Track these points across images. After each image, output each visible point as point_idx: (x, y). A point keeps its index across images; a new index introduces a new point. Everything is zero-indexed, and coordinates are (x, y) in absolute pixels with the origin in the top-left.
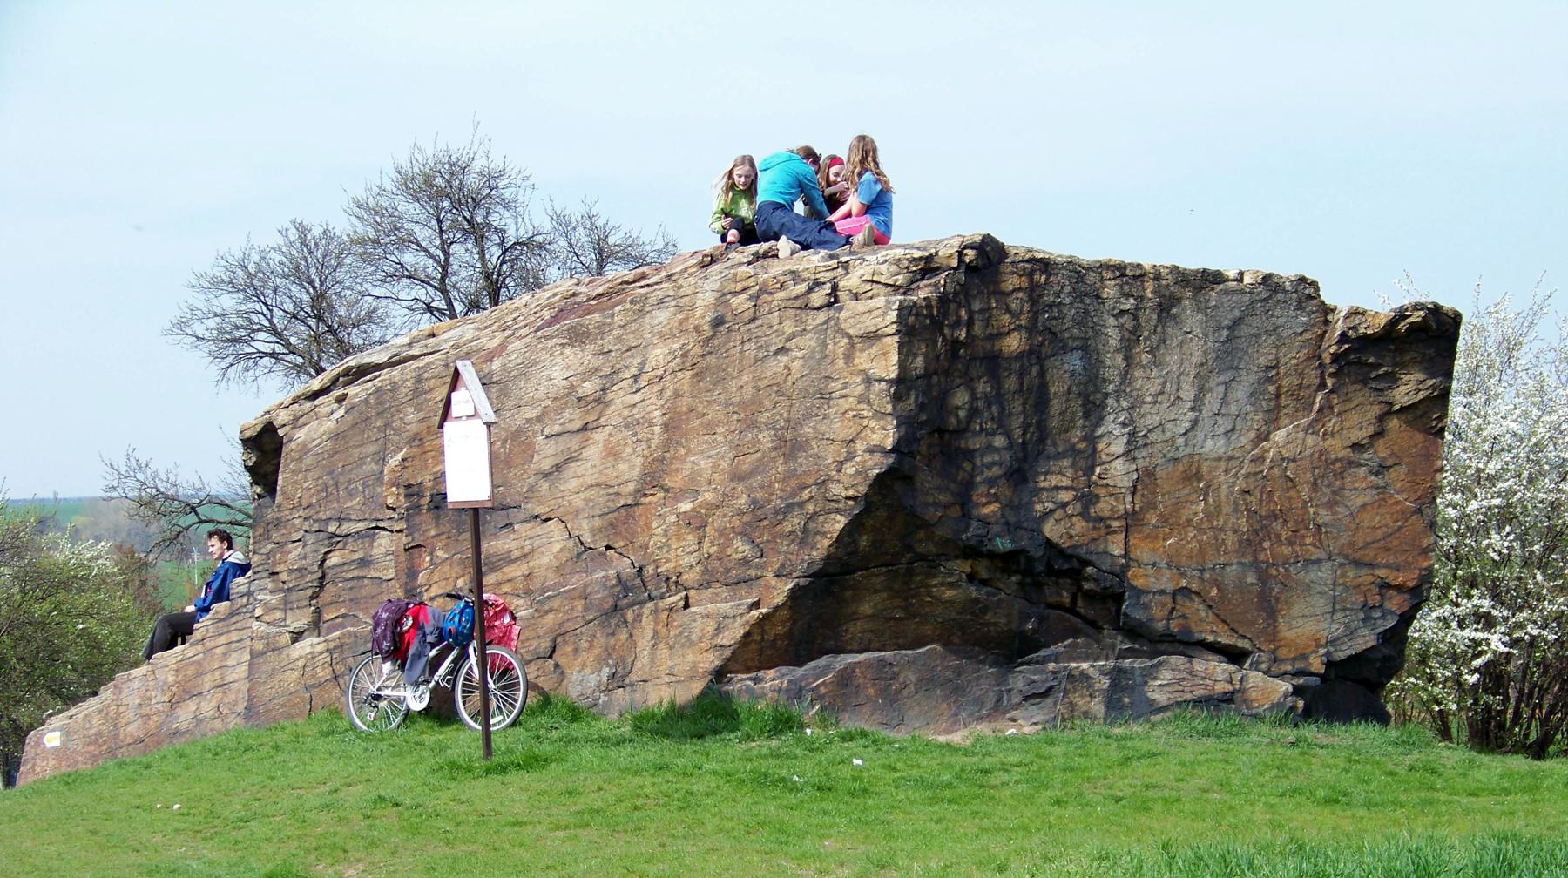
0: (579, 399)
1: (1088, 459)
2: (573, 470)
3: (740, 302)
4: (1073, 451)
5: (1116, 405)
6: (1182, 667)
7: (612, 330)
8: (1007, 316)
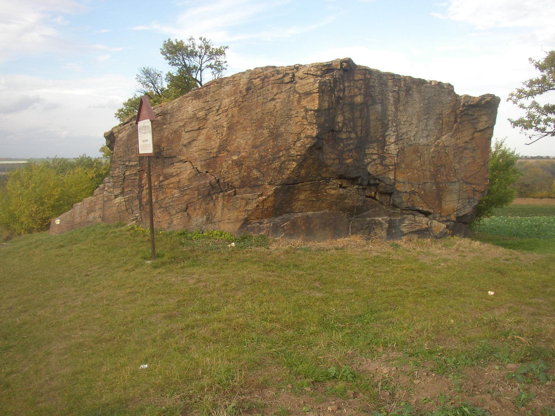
0: (197, 118)
1: (383, 144)
2: (194, 144)
3: (257, 82)
4: (377, 140)
5: (391, 124)
6: (412, 219)
7: (209, 94)
8: (357, 89)
